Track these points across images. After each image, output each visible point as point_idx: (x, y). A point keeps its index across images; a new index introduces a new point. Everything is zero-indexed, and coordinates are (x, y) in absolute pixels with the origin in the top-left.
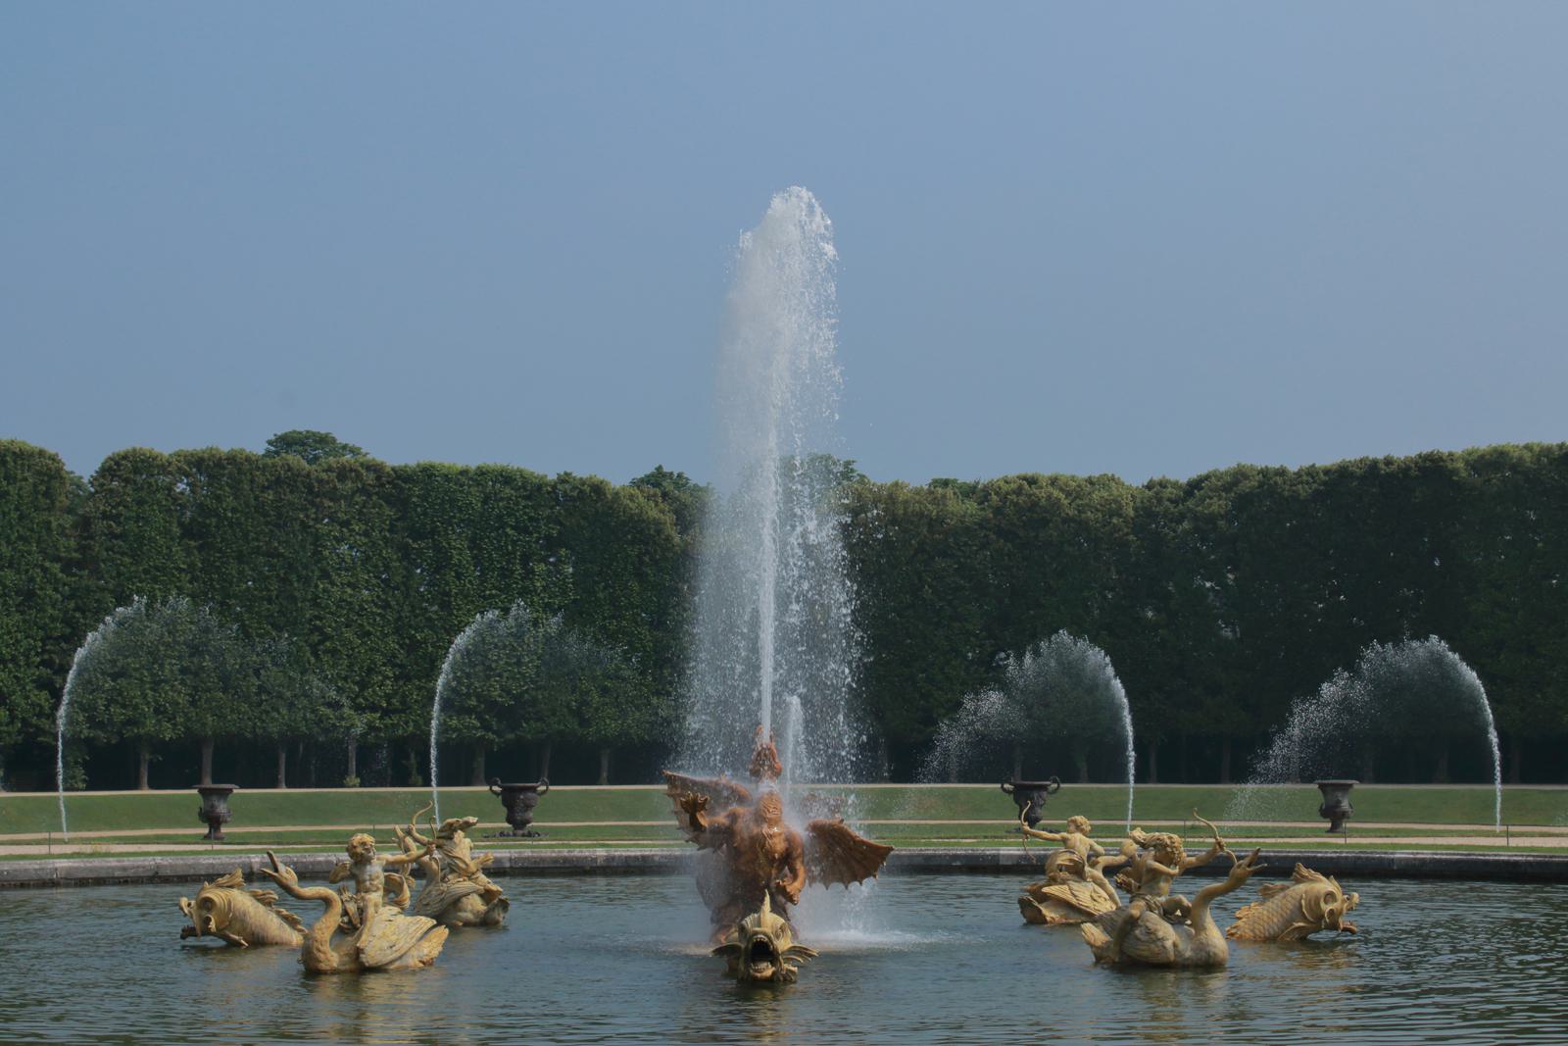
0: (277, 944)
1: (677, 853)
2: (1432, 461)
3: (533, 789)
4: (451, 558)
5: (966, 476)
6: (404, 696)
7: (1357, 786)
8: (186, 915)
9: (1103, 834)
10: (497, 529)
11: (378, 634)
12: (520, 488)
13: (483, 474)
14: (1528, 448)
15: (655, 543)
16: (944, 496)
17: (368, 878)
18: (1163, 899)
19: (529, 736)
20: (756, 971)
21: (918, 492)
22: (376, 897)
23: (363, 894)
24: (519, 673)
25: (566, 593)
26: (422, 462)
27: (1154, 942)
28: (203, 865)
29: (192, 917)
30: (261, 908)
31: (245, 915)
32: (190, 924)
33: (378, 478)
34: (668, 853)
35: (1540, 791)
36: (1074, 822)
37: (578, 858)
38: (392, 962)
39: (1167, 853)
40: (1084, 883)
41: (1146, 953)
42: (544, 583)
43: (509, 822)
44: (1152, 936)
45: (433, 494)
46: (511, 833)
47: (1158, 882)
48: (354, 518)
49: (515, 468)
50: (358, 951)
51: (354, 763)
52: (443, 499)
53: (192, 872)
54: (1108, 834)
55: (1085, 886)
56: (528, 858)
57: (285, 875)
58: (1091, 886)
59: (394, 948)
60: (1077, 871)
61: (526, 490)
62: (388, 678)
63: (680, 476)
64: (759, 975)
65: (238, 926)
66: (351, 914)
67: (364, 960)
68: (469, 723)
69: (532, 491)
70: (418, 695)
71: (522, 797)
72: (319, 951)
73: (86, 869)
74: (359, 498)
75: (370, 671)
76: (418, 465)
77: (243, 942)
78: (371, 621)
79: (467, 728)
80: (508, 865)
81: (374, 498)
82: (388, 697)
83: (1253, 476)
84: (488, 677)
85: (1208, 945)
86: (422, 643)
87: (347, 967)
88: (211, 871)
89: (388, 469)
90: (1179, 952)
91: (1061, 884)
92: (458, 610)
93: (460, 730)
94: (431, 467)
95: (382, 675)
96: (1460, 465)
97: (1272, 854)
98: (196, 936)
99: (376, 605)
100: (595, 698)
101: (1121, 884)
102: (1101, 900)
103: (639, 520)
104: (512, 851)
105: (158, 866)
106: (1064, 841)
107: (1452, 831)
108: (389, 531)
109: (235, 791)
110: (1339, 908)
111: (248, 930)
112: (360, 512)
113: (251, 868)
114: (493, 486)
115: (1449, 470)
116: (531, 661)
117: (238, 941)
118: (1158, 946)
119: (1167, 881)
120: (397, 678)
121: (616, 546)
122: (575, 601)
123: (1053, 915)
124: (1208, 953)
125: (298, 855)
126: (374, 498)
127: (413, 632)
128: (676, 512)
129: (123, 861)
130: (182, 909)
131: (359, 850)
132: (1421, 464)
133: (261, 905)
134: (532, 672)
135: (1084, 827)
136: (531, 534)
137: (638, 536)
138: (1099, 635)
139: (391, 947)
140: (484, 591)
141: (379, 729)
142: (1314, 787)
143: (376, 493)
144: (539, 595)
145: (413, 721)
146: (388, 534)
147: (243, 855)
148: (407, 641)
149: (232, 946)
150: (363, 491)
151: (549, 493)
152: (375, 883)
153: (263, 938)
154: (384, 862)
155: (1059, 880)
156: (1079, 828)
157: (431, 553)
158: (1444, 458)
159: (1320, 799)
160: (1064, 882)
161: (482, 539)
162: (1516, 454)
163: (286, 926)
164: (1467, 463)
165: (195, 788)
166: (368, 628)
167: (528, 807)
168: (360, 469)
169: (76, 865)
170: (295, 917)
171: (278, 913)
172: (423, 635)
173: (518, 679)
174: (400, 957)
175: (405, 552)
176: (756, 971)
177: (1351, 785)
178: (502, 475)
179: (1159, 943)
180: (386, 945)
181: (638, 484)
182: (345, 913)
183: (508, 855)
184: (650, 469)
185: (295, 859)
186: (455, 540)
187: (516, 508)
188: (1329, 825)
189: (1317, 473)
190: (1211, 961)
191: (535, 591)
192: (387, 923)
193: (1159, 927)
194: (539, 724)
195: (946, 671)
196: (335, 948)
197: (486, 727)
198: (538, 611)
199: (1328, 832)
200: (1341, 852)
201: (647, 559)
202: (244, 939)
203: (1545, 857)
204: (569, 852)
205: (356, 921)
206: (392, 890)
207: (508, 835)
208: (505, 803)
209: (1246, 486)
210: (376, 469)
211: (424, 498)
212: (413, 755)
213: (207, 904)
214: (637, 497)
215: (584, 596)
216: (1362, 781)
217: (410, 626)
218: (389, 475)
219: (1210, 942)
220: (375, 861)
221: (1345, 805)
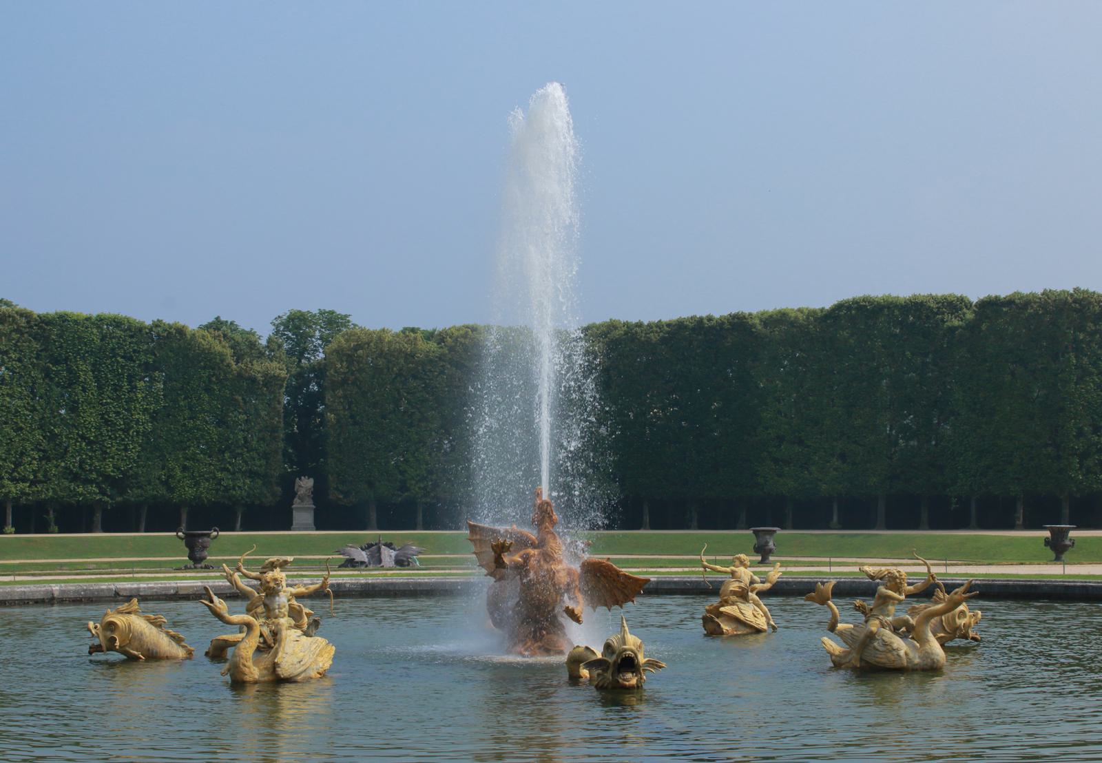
0: (167, 658)
1: (362, 581)
2: (738, 318)
3: (208, 535)
4: (79, 377)
5: (426, 325)
6: (46, 471)
7: (779, 532)
8: (93, 635)
9: (677, 566)
10: (111, 358)
11: (28, 429)
12: (126, 330)
13: (101, 320)
14: (800, 310)
15: (219, 368)
16: (415, 339)
17: (277, 607)
18: (890, 619)
19: (133, 499)
20: (624, 680)
21: (397, 335)
22: (285, 621)
23: (274, 620)
24: (126, 456)
25: (158, 402)
26: (58, 311)
27: (890, 651)
29: (98, 637)
30: (154, 630)
31: (142, 635)
32: (96, 642)
33: (28, 322)
34: (356, 581)
35: (812, 535)
36: (739, 559)
38: (299, 675)
39: (896, 583)
40: (748, 604)
41: (883, 661)
42: (144, 395)
44: (889, 647)
45: (67, 334)
46: (193, 567)
47: (887, 606)
48: (11, 349)
49: (124, 316)
50: (275, 666)
51: (11, 518)
52: (74, 337)
53: (9, 598)
54: (653, 565)
55: (748, 606)
57: (219, 605)
58: (752, 606)
59: (302, 663)
60: (743, 595)
61: (131, 331)
62: (36, 459)
63: (232, 323)
64: (627, 683)
65: (136, 644)
66: (265, 636)
67: (280, 673)
68: (91, 490)
69: (135, 331)
70: (55, 471)
71: (200, 541)
72: (245, 666)
74: (15, 336)
75: (22, 454)
76: (56, 313)
77: (142, 657)
78: (23, 420)
79: (89, 493)
81: (26, 335)
82: (35, 473)
83: (621, 328)
84: (105, 459)
85: (932, 654)
86: (59, 435)
87: (266, 678)
88: (23, 597)
89: (35, 316)
90: (910, 659)
91: (731, 605)
92: (84, 413)
94: (65, 314)
95: (31, 457)
96: (757, 321)
97: (790, 580)
98: (103, 651)
99: (27, 409)
100: (179, 474)
101: (859, 607)
102: (759, 616)
103: (209, 353)
106: (733, 573)
108: (36, 358)
109: (778, 532)
110: (968, 622)
111: (145, 647)
112: (16, 345)
114: (108, 328)
115: (749, 325)
116: (134, 448)
117: (135, 656)
118: (893, 655)
119: (893, 604)
120: (41, 459)
121: (193, 370)
122: (164, 407)
123: (727, 628)
124: (932, 660)
126: (26, 335)
127: (52, 428)
128: (232, 347)
130: (89, 630)
131: (272, 584)
132: (731, 320)
133: (153, 627)
134: (134, 456)
135: (746, 562)
136: (134, 361)
137: (208, 363)
138: (725, 425)
139: (300, 662)
140: (101, 400)
141: (29, 494)
142: (750, 532)
143: (27, 332)
144: (140, 403)
145: (52, 489)
146: (35, 360)
147: (46, 585)
148: (48, 434)
149: (132, 659)
150: (18, 331)
151: (147, 333)
152: (283, 610)
153: (157, 653)
154: (289, 594)
155: (730, 602)
156: (742, 563)
157: (65, 374)
158: (747, 316)
159: (755, 541)
160: (733, 604)
161: (100, 365)
162: (793, 315)
163: (173, 643)
164: (761, 320)
165: (1045, 529)
166: (21, 425)
167: (204, 548)
168: (16, 315)
170: (180, 636)
171: (167, 633)
172: (59, 430)
173: (125, 460)
174: (305, 670)
175: (47, 374)
176: (624, 680)
177: (775, 531)
178: (114, 321)
179: (895, 653)
180: (296, 660)
181: (208, 327)
182: (261, 635)
184: (211, 319)
185: (85, 588)
186: (82, 365)
187: (124, 344)
188: (759, 558)
189: (663, 326)
190: (935, 666)
191: (138, 400)
193: (893, 640)
194: (139, 490)
195: (416, 455)
196: (256, 663)
197: (103, 493)
198: (139, 414)
199: (759, 563)
200: (840, 578)
201: (214, 379)
202: (142, 654)
203: (988, 580)
205: (270, 641)
206: (295, 614)
207: (190, 568)
208: (187, 545)
209: (616, 334)
210: (26, 315)
211: (60, 336)
212: (51, 512)
213: (111, 626)
214: (208, 338)
215: (171, 404)
216: (783, 528)
217: (51, 424)
218: (36, 320)
219: (934, 652)
220: (281, 594)
221: (771, 544)
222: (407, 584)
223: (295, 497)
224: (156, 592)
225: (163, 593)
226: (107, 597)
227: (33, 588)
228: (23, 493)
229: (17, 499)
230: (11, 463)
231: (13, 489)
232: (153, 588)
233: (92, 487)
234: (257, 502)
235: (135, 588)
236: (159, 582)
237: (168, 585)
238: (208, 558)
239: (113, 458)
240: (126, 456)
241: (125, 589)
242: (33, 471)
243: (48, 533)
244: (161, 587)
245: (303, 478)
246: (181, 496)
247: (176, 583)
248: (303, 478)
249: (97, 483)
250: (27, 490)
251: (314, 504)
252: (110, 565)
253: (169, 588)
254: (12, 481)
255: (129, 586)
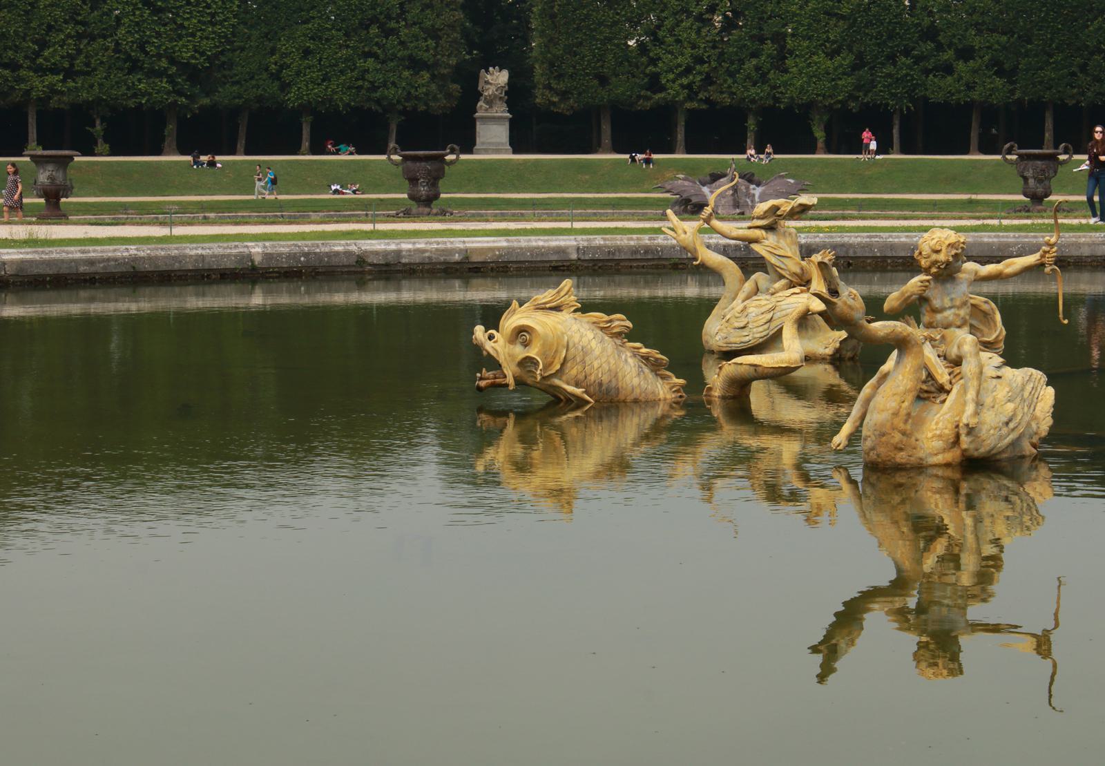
28: (191, 256)
37: (664, 248)
43: (1025, 195)
56: (599, 247)
59: (1011, 425)
73: (44, 262)
80: (574, 256)
82: (72, 58)
93: (150, 94)
104: (579, 238)
105: (136, 259)
107: (125, 207)
109: (76, 159)
113: (252, 261)
125: (309, 243)
129: (89, 252)
139: (1007, 424)
141: (62, 93)
163: (647, 370)
169: (29, 257)
183: (575, 243)
192: (995, 381)
194: (235, 88)
204: (650, 239)
222: (869, 246)
223: (478, 101)
224: (429, 257)
225: (442, 259)
226: (343, 266)
227: (216, 249)
228: (53, 90)
229: (43, 101)
230: (34, 43)
231: (39, 85)
232: (424, 251)
233: (161, 81)
234: (422, 108)
235: (394, 251)
236: (433, 240)
237: (449, 246)
238: (443, 196)
239: (193, 35)
240: (214, 32)
241: (377, 253)
242: (69, 55)
243: (93, 154)
244: (437, 250)
245: (491, 69)
246: (302, 98)
247: (464, 242)
248: (491, 69)
249: (169, 76)
250: (59, 87)
251: (509, 112)
252: (203, 207)
253: (451, 252)
254: (36, 71)
255: (383, 247)
